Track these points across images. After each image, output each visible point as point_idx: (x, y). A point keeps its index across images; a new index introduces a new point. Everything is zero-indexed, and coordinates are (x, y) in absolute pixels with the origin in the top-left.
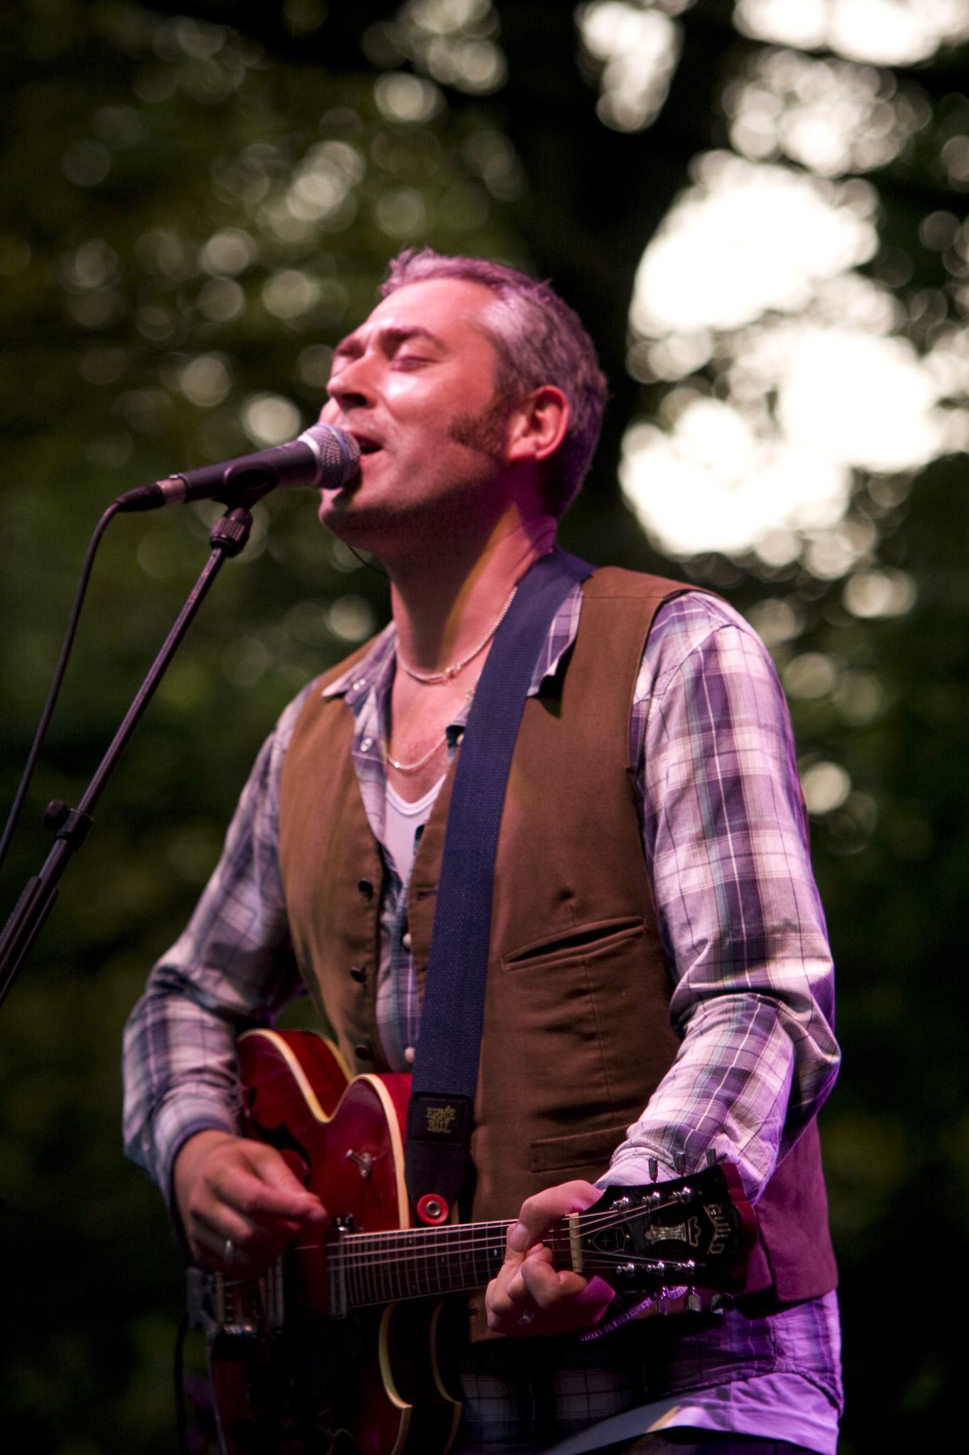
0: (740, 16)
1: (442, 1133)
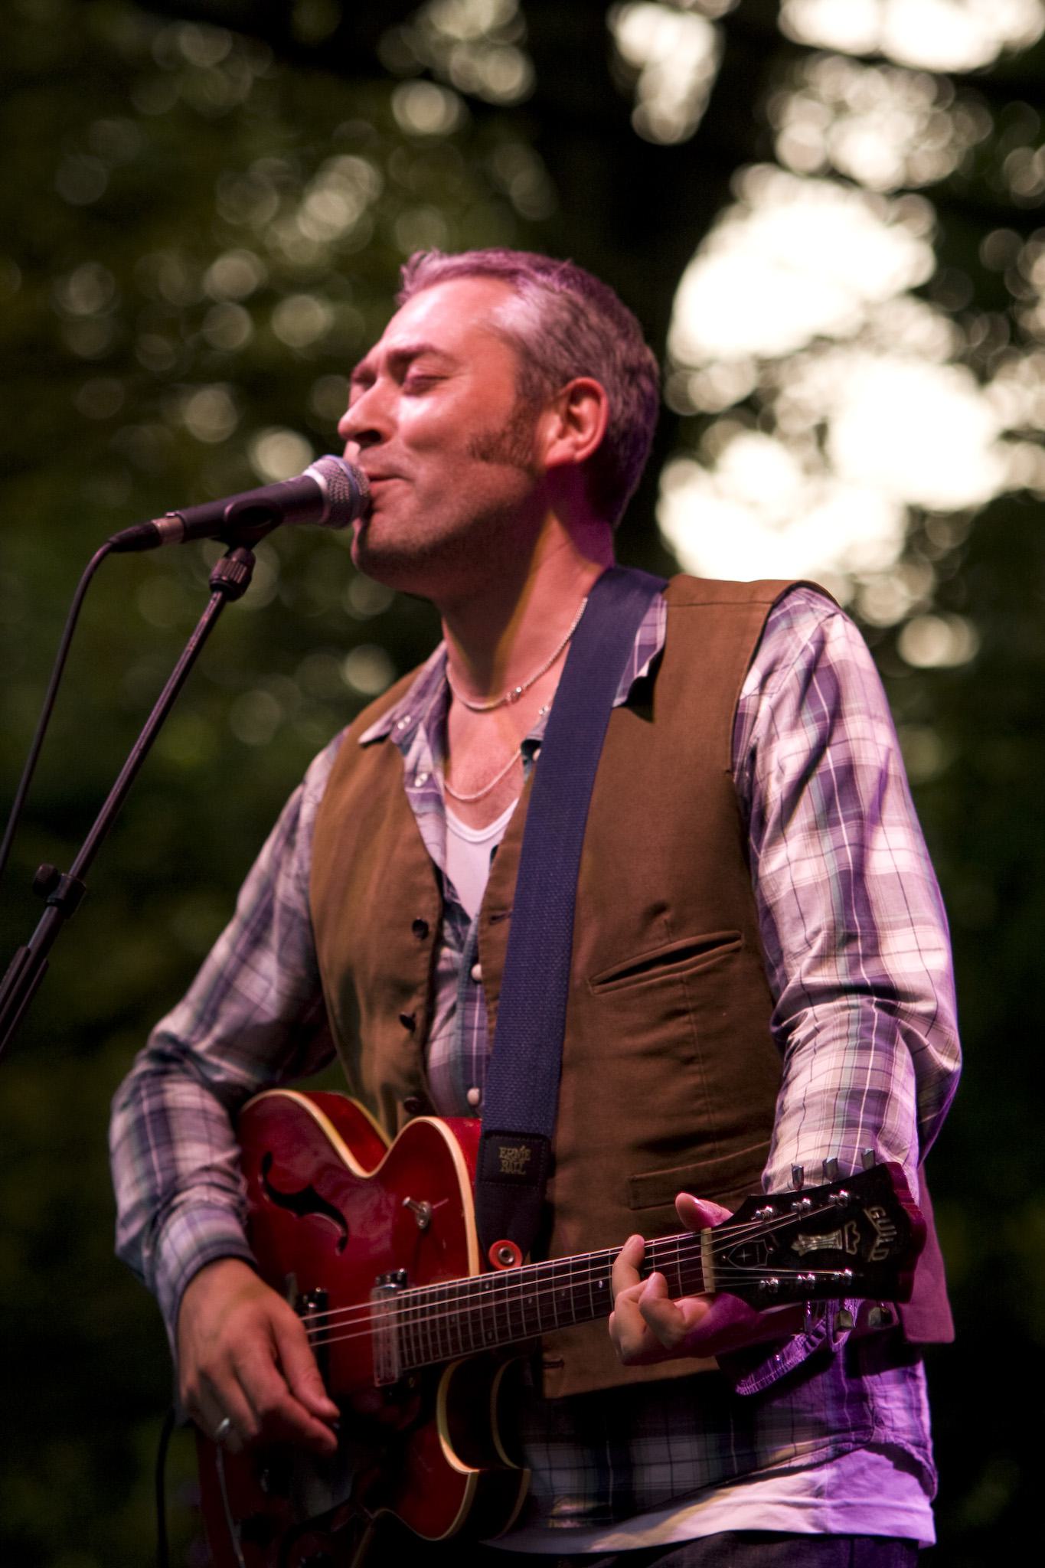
0: (786, 20)
1: (517, 1176)
